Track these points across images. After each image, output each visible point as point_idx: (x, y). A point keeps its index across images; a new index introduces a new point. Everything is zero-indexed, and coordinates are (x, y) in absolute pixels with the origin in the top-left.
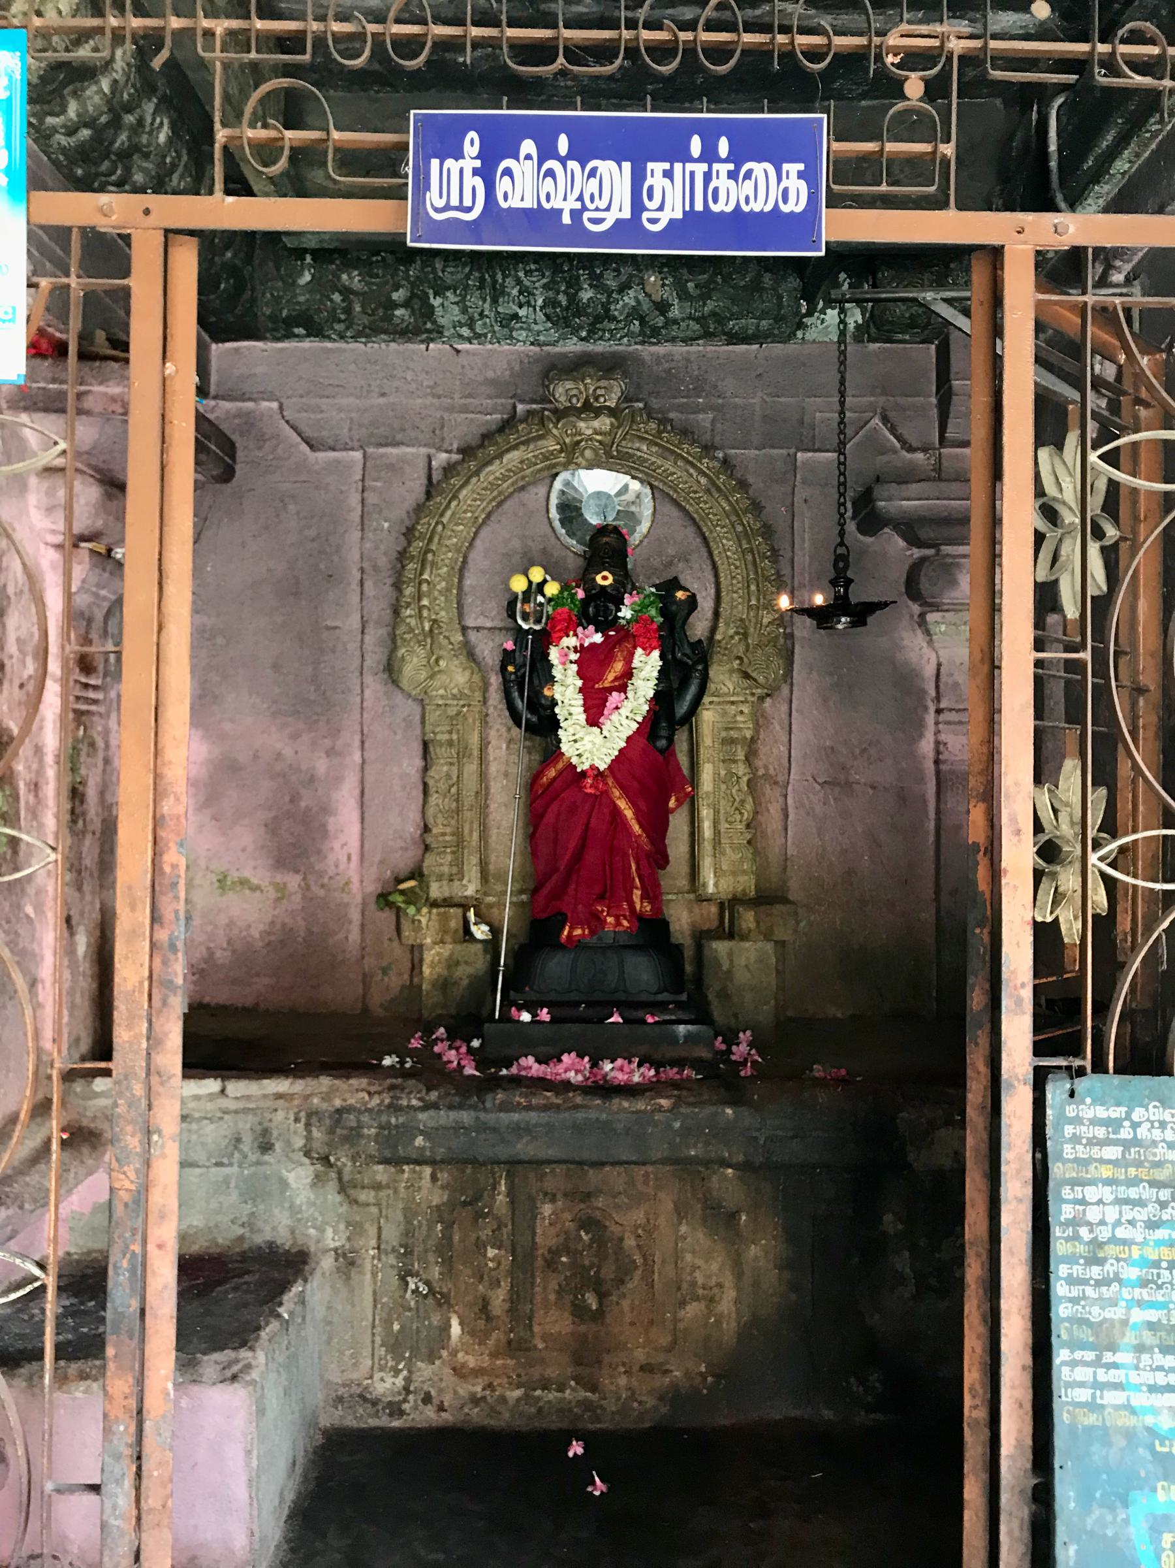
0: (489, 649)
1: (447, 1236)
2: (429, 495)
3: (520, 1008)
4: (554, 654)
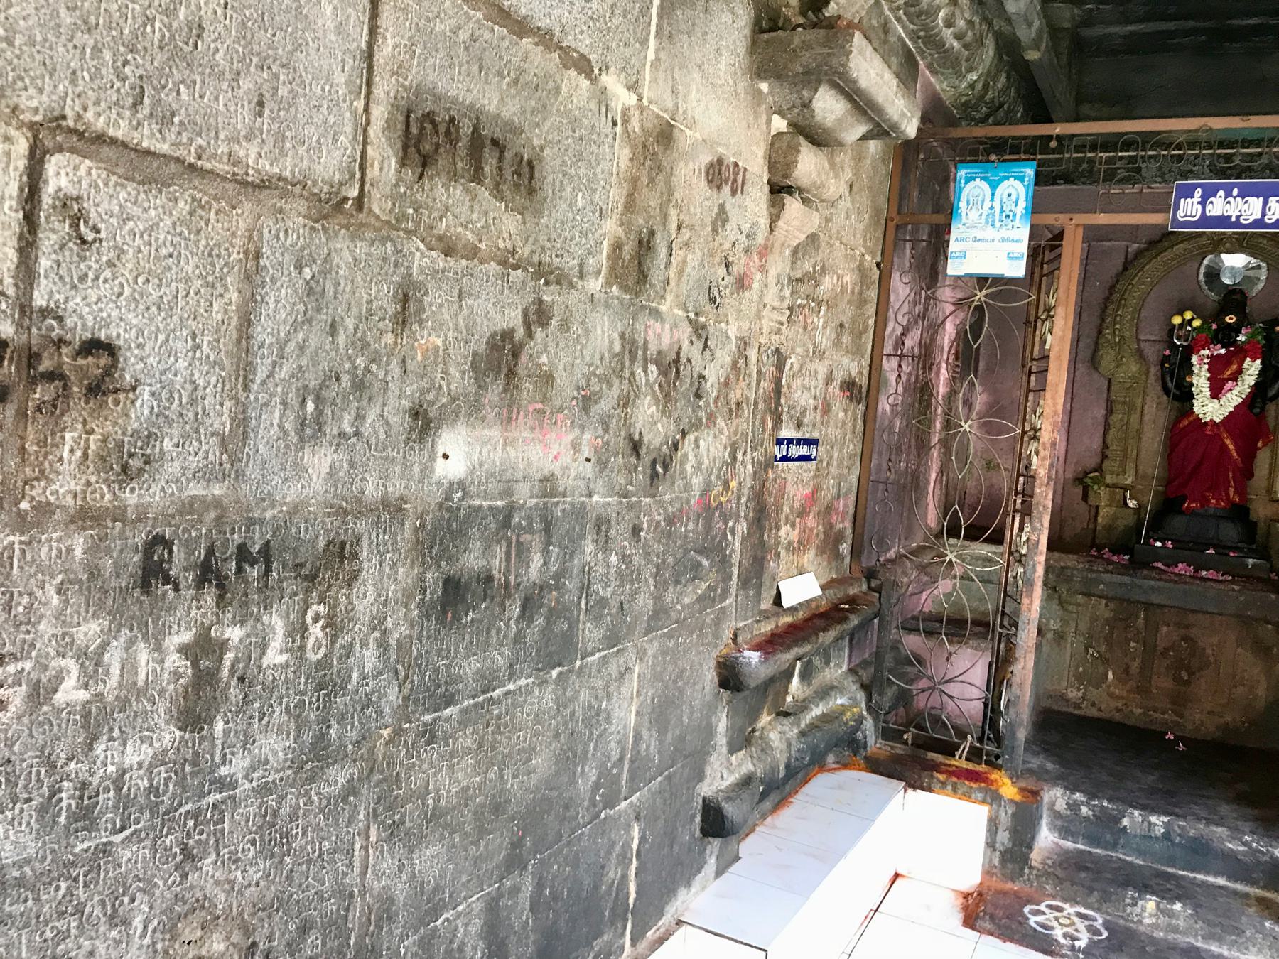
0: (1152, 352)
1: (1111, 633)
2: (1125, 269)
3: (1156, 540)
4: (1195, 359)
